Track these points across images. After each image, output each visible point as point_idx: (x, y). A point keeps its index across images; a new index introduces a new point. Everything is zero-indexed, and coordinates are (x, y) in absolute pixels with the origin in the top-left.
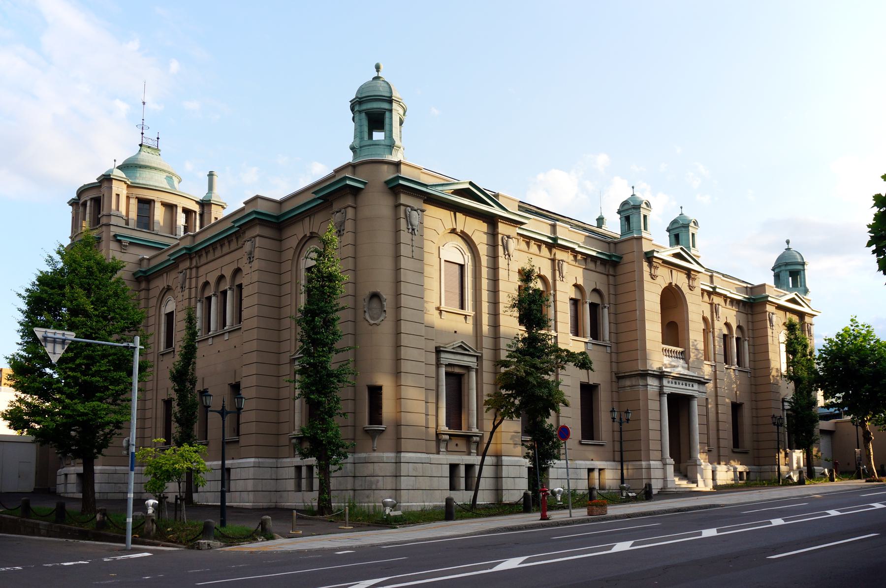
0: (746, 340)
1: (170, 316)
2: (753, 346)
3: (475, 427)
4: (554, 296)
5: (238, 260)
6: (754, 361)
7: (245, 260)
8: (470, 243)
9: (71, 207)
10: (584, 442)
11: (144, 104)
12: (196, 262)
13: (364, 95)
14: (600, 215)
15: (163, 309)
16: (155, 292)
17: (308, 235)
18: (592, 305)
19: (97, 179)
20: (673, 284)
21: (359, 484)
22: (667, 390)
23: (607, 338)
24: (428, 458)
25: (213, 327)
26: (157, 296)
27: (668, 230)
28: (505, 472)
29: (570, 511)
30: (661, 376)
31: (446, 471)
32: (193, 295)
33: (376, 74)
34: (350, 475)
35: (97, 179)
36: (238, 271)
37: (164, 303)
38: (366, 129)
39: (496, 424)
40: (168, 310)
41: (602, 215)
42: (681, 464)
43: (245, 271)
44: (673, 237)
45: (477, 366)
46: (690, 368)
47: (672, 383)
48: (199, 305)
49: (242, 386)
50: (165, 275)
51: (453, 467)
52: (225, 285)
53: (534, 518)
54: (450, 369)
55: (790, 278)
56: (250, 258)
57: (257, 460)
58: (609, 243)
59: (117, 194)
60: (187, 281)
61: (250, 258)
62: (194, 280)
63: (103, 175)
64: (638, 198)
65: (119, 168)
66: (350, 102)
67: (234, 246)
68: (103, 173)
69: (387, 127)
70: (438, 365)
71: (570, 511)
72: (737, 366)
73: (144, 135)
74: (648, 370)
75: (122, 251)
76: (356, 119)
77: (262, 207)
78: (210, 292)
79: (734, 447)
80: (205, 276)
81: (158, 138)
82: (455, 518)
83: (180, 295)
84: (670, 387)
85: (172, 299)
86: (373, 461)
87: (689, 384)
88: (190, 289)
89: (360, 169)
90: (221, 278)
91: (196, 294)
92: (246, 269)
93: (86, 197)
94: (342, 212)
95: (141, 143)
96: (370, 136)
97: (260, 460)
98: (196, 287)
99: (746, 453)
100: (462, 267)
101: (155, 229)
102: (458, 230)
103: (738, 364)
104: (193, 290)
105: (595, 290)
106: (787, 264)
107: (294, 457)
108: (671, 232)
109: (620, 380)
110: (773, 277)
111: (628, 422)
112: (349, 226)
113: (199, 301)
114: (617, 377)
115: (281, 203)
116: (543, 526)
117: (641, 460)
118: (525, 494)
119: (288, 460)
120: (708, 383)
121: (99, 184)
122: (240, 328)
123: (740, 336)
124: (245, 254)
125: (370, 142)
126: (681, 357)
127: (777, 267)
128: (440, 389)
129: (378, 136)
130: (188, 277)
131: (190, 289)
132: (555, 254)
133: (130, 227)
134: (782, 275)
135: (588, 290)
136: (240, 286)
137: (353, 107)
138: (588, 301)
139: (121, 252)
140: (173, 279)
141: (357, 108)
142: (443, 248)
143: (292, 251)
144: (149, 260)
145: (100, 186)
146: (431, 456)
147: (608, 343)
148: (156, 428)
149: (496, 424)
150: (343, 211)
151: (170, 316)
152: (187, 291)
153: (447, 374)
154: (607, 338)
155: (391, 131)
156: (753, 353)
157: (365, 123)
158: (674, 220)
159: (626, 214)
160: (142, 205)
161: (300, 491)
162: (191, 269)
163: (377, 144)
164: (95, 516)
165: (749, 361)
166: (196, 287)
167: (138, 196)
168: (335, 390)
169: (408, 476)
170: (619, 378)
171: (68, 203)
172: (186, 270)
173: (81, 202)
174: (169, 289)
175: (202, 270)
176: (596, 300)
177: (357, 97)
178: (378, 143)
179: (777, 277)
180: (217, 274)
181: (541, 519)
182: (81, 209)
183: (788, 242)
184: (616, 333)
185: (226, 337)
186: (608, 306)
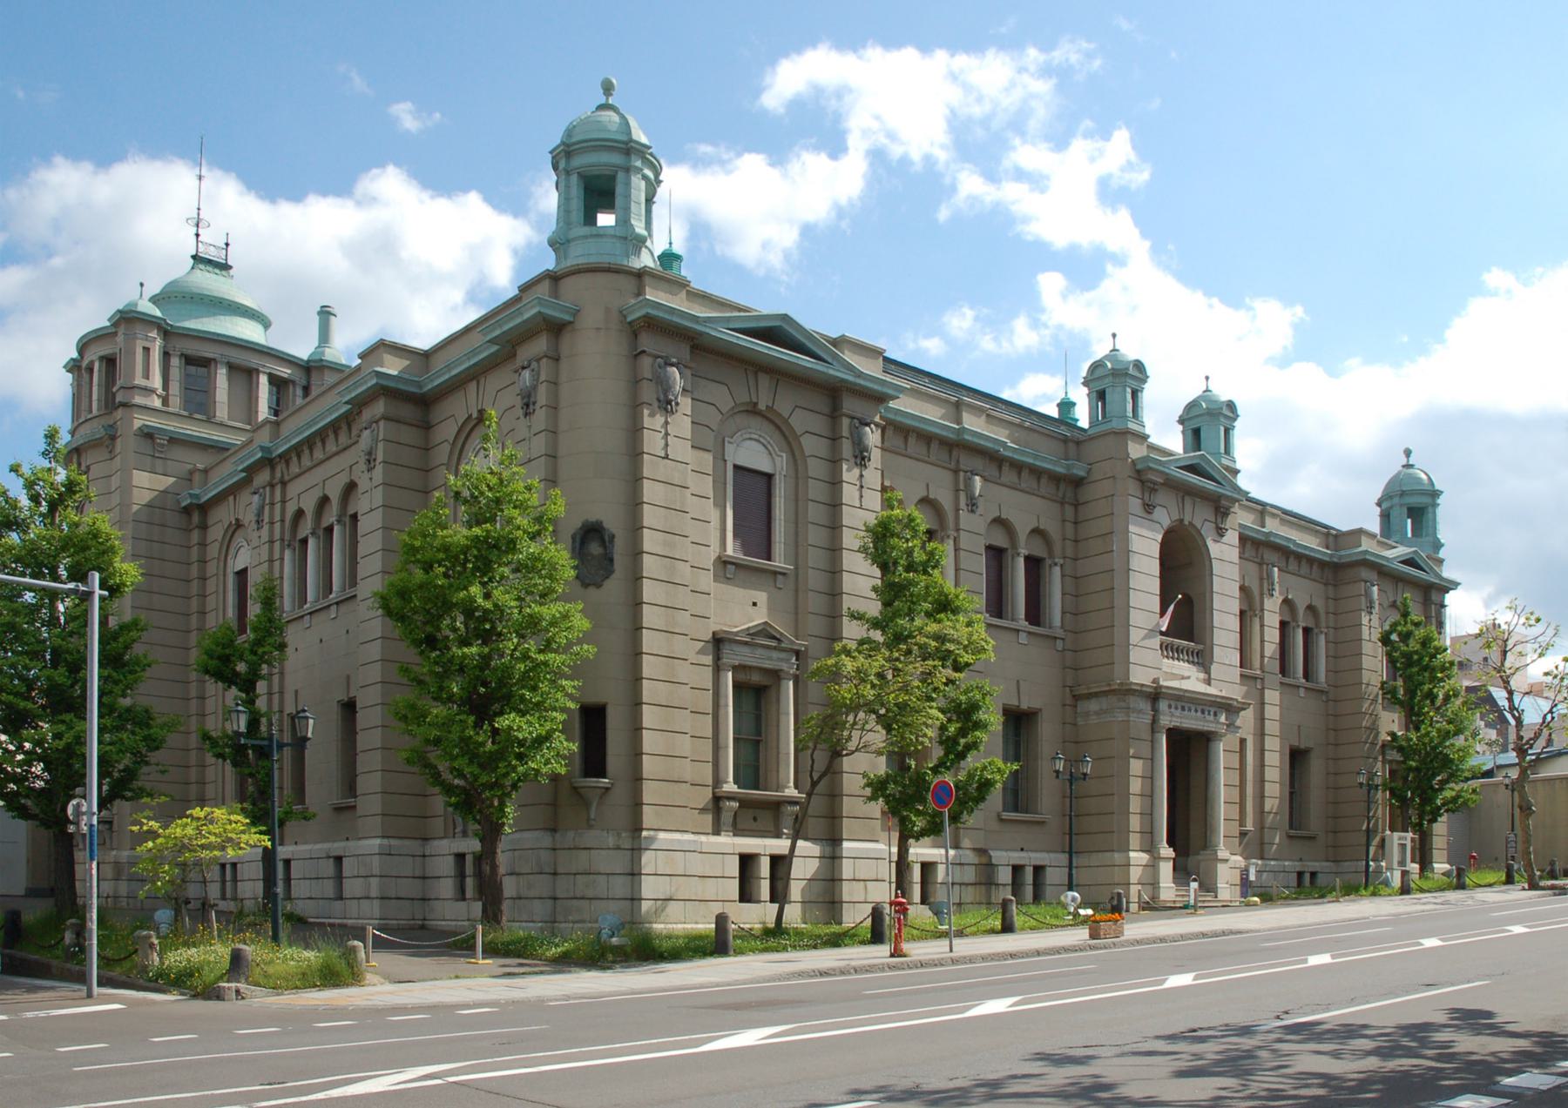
0: (1322, 632)
1: (242, 574)
2: (1334, 643)
3: (792, 784)
4: (955, 541)
5: (351, 467)
6: (1336, 672)
7: (363, 466)
8: (787, 433)
9: (70, 375)
10: (1006, 815)
11: (200, 179)
12: (282, 473)
13: (574, 140)
14: (1063, 396)
15: (230, 562)
16: (216, 533)
17: (475, 415)
18: (1028, 559)
19: (109, 320)
20: (1186, 523)
21: (563, 887)
22: (1166, 721)
23: (1057, 621)
24: (694, 841)
25: (310, 596)
26: (220, 539)
27: (1181, 421)
28: (847, 870)
29: (951, 942)
30: (1155, 695)
31: (733, 868)
32: (277, 536)
33: (602, 100)
34: (547, 870)
35: (109, 320)
36: (351, 487)
37: (232, 551)
38: (577, 204)
39: (815, 779)
40: (239, 567)
41: (1069, 396)
42: (1191, 858)
43: (361, 488)
44: (1189, 433)
45: (797, 669)
46: (1213, 682)
47: (1176, 708)
48: (288, 554)
49: (359, 705)
50: (231, 498)
51: (747, 861)
52: (330, 517)
53: (881, 952)
54: (742, 677)
55: (1409, 521)
56: (369, 461)
57: (385, 841)
58: (1065, 440)
59: (144, 348)
60: (267, 508)
61: (369, 461)
62: (278, 507)
63: (119, 311)
64: (1123, 355)
65: (155, 300)
66: (551, 152)
67: (343, 439)
68: (121, 308)
69: (619, 201)
70: (717, 669)
71: (951, 942)
72: (1304, 681)
73: (200, 239)
74: (1132, 683)
75: (157, 455)
76: (562, 185)
77: (392, 367)
78: (306, 528)
79: (1291, 827)
80: (296, 500)
81: (227, 245)
82: (732, 952)
83: (256, 534)
84: (1171, 718)
85: (245, 543)
86: (588, 846)
87: (1209, 712)
88: (272, 523)
89: (568, 285)
90: (324, 501)
91: (282, 532)
92: (363, 484)
93: (93, 355)
94: (532, 367)
95: (194, 253)
96: (590, 220)
97: (393, 842)
98: (282, 521)
99: (1312, 838)
100: (769, 477)
101: (217, 414)
102: (762, 407)
103: (1306, 675)
104: (277, 526)
105: (1036, 531)
106: (1403, 494)
107: (454, 837)
108: (1186, 423)
109: (1079, 703)
110: (1379, 518)
111: (1084, 779)
112: (542, 397)
113: (289, 546)
114: (1074, 696)
115: (426, 356)
116: (892, 967)
117: (1113, 851)
118: (873, 909)
119: (445, 842)
120: (1244, 709)
121: (114, 330)
122: (355, 596)
123: (1311, 624)
124: (362, 454)
125: (586, 230)
126: (1196, 660)
127: (1386, 500)
128: (722, 712)
129: (605, 220)
130: (267, 501)
131: (272, 523)
132: (958, 461)
133: (170, 409)
134: (1394, 513)
135: (1022, 530)
136: (354, 517)
137: (557, 163)
138: (1023, 551)
139: (153, 456)
140: (247, 506)
141: (562, 165)
142: (731, 440)
143: (446, 448)
144: (206, 471)
145: (115, 334)
146: (703, 838)
147: (1059, 633)
148: (223, 782)
149: (815, 779)
150: (534, 365)
151: (242, 574)
152: (266, 527)
153: (738, 686)
154: (1057, 621)
155: (627, 210)
156: (1333, 657)
157: (576, 191)
158: (1193, 401)
159: (1099, 386)
160: (192, 369)
161: (464, 899)
162: (272, 486)
163: (603, 233)
164: (63, 938)
165: (1327, 671)
166: (282, 521)
167: (185, 351)
168: (134, 634)
169: (656, 875)
170: (1077, 698)
171: (65, 367)
172: (264, 488)
173: (84, 364)
174: (239, 525)
175: (293, 489)
176: (1039, 551)
177: (563, 143)
178: (602, 233)
179: (1385, 517)
180: (316, 495)
181: (892, 956)
182: (86, 376)
183: (1408, 453)
184: (1073, 612)
185: (333, 611)
186: (1061, 561)
